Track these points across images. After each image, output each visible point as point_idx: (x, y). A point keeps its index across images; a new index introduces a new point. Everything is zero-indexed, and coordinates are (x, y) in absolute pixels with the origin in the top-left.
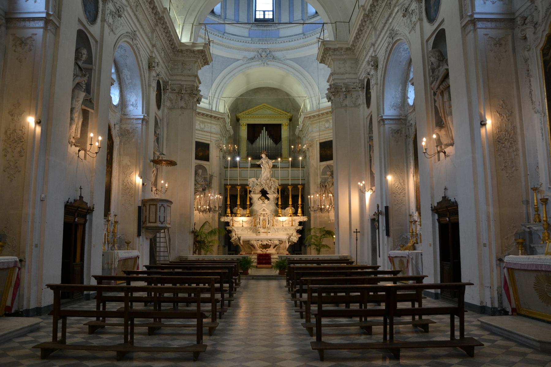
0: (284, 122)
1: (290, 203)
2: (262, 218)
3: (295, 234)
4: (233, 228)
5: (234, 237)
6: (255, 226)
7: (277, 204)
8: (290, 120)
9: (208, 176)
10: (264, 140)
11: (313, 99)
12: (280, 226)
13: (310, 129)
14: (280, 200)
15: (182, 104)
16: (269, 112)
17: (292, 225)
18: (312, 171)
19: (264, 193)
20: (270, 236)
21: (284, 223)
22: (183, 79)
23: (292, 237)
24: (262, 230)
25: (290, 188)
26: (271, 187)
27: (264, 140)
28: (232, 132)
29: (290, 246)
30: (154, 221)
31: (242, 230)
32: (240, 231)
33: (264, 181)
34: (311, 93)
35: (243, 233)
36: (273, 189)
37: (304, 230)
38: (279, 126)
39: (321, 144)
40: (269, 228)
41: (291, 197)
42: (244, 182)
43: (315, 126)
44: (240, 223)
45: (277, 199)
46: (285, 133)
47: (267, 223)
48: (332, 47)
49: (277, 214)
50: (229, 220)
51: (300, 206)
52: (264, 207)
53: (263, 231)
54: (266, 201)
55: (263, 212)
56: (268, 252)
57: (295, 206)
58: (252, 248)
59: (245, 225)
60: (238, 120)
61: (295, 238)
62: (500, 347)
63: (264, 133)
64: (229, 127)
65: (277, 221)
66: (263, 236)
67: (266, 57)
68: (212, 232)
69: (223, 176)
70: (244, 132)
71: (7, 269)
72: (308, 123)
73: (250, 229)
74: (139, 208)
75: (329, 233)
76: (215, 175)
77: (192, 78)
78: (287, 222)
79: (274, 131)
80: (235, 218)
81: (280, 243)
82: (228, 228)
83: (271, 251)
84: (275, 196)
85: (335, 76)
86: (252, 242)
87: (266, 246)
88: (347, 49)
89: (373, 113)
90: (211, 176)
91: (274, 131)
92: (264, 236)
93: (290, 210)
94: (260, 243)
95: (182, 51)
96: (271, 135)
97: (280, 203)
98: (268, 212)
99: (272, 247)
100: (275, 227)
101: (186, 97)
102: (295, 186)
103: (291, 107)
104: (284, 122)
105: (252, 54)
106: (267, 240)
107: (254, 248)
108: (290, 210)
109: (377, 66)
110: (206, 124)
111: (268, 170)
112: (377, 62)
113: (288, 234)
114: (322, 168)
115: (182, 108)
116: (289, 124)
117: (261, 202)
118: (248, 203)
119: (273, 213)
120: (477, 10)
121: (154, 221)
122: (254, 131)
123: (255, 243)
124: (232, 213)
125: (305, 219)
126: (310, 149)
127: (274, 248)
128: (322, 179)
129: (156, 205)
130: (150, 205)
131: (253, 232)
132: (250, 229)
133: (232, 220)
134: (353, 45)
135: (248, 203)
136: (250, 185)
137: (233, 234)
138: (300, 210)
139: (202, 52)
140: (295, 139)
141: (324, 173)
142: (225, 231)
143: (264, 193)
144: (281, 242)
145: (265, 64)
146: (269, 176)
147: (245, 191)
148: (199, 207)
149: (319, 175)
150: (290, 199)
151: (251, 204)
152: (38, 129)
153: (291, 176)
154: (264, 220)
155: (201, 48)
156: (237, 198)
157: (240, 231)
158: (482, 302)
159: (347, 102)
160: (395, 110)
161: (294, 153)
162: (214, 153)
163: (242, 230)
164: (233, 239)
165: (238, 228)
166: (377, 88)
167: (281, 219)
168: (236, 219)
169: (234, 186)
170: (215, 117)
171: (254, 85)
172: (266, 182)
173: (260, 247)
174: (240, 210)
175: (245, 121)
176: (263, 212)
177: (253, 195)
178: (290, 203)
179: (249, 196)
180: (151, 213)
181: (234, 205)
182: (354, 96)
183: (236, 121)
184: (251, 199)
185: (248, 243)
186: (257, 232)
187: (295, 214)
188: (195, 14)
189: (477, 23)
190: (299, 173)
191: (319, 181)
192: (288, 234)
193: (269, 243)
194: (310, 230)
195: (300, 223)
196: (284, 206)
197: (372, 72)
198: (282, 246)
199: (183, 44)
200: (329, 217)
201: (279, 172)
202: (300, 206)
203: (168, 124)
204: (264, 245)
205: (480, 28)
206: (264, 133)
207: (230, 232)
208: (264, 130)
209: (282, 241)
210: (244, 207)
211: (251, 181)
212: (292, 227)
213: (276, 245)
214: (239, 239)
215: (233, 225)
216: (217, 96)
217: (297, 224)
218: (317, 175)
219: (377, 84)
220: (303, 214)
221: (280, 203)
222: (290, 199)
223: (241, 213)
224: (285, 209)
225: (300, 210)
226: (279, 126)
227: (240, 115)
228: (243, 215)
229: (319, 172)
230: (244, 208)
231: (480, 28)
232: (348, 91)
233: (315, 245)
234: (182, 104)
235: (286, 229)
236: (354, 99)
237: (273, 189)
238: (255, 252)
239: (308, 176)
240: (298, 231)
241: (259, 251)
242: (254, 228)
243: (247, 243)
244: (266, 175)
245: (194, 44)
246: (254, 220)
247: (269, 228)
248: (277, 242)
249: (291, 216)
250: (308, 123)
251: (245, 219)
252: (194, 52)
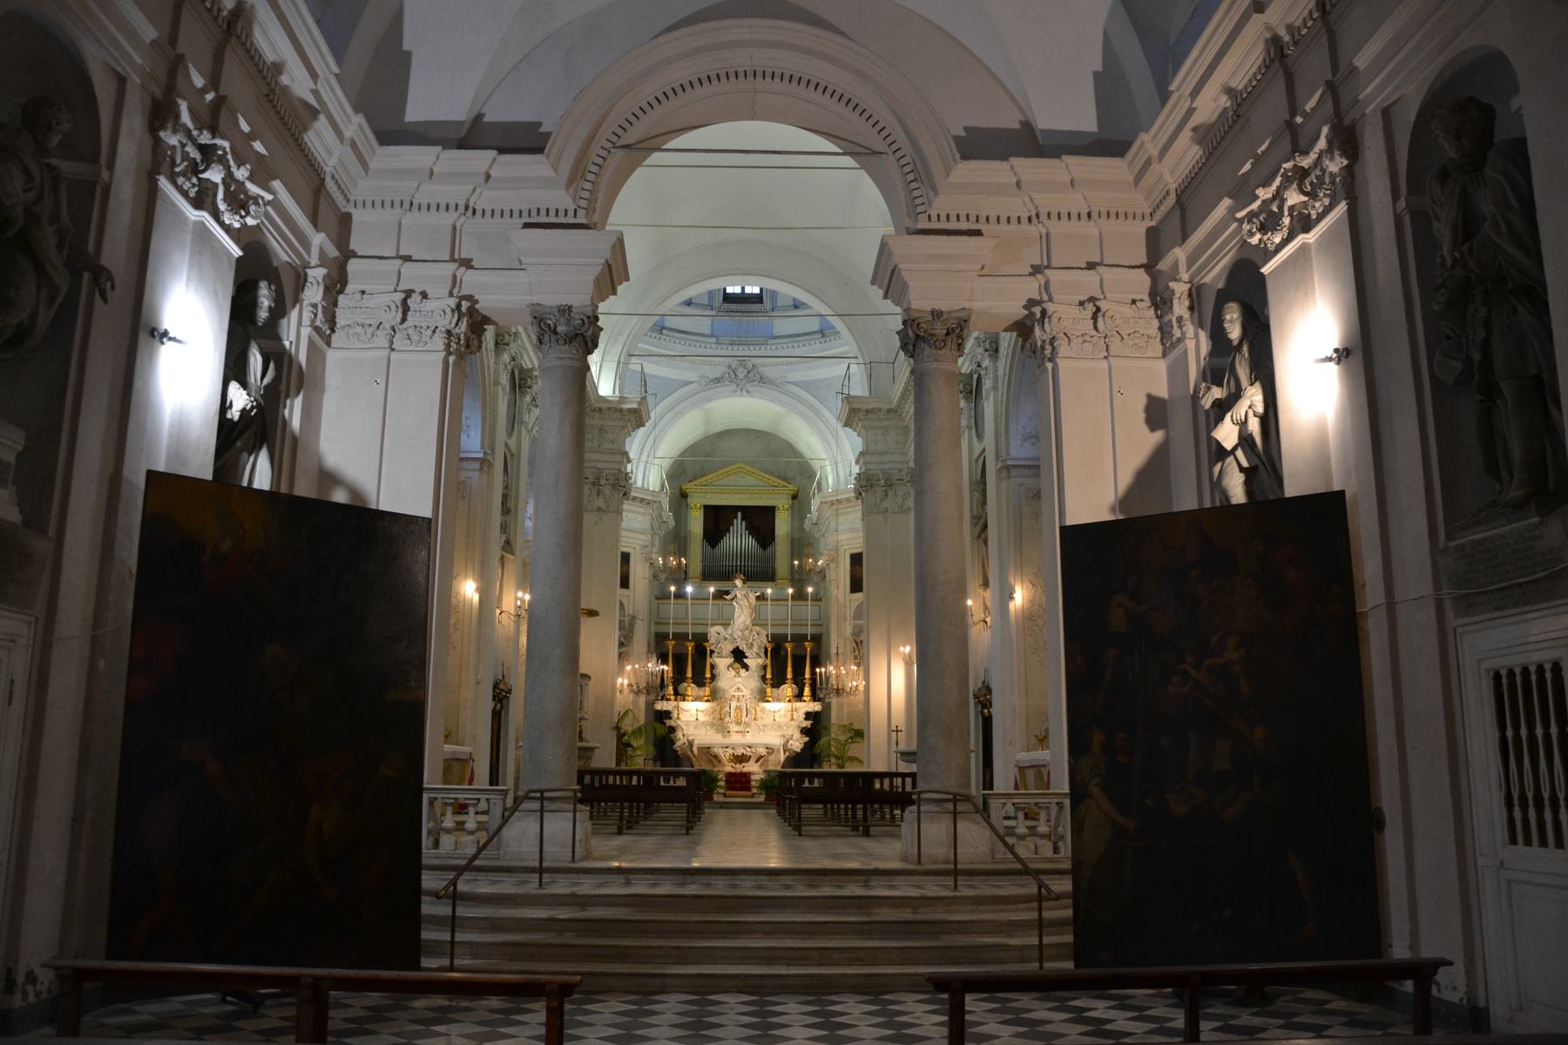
0: (781, 502)
1: (789, 676)
2: (734, 704)
3: (797, 735)
5: (681, 739)
7: (764, 678)
8: (794, 497)
10: (738, 539)
11: (840, 465)
12: (768, 720)
13: (832, 526)
14: (769, 670)
15: (600, 502)
16: (750, 480)
18: (834, 610)
19: (738, 655)
20: (749, 738)
22: (602, 458)
24: (734, 728)
25: (789, 646)
27: (738, 539)
28: (672, 523)
29: (787, 759)
34: (835, 458)
36: (755, 648)
37: (815, 727)
38: (770, 512)
40: (747, 725)
41: (793, 660)
42: (700, 630)
44: (692, 716)
45: (765, 667)
46: (782, 525)
48: (863, 407)
49: (763, 697)
51: (807, 682)
52: (738, 684)
54: (743, 671)
56: (745, 770)
57: (798, 681)
59: (702, 718)
60: (684, 496)
61: (797, 744)
63: (739, 525)
64: (668, 515)
65: (763, 710)
66: (735, 739)
67: (746, 377)
68: (638, 732)
69: (657, 618)
70: (696, 523)
71: (1532, 584)
72: (828, 512)
75: (859, 734)
77: (618, 458)
79: (760, 521)
82: (668, 722)
83: (752, 767)
84: (761, 661)
85: (868, 458)
87: (742, 759)
88: (889, 411)
89: (987, 453)
90: (633, 618)
91: (760, 521)
92: (739, 739)
93: (788, 689)
94: (730, 751)
95: (600, 410)
96: (753, 530)
97: (769, 676)
98: (746, 692)
99: (753, 760)
100: (760, 722)
101: (607, 491)
102: (799, 639)
103: (796, 474)
104: (781, 502)
105: (718, 372)
106: (744, 746)
108: (788, 689)
109: (997, 351)
111: (747, 611)
112: (997, 343)
114: (854, 606)
115: (599, 509)
116: (792, 507)
117: (733, 673)
118: (708, 675)
120: (1013, 453)
122: (718, 520)
123: (719, 751)
124: (676, 693)
125: (816, 707)
126: (832, 566)
128: (855, 626)
131: (718, 731)
132: (712, 725)
133: (677, 707)
134: (898, 406)
135: (708, 675)
136: (712, 640)
137: (680, 735)
138: (807, 690)
139: (635, 411)
140: (802, 544)
142: (661, 728)
143: (738, 655)
144: (770, 750)
146: (748, 622)
147: (702, 652)
148: (621, 677)
150: (789, 669)
151: (713, 677)
152: (476, 598)
153: (790, 616)
154: (738, 708)
155: (635, 406)
156: (688, 661)
159: (886, 504)
161: (798, 579)
162: (639, 572)
164: (678, 744)
165: (687, 723)
166: (995, 399)
167: (771, 706)
168: (684, 705)
169: (681, 637)
170: (642, 500)
171: (719, 427)
174: (691, 689)
175: (702, 497)
177: (717, 661)
178: (789, 676)
179: (709, 661)
181: (679, 677)
182: (900, 493)
183: (681, 499)
184: (713, 667)
186: (725, 731)
187: (799, 696)
188: (622, 339)
190: (808, 610)
191: (849, 631)
193: (748, 752)
194: (827, 729)
195: (808, 715)
196: (778, 681)
197: (986, 363)
198: (771, 758)
199: (603, 399)
201: (769, 609)
202: (807, 682)
206: (739, 525)
207: (672, 730)
208: (740, 529)
210: (699, 681)
211: (713, 631)
214: (691, 744)
216: (649, 462)
219: (995, 388)
220: (814, 698)
221: (769, 676)
222: (789, 669)
225: (807, 690)
226: (770, 512)
227: (688, 487)
228: (697, 699)
229: (850, 613)
232: (890, 485)
234: (600, 502)
235: (780, 726)
237: (755, 648)
239: (828, 619)
240: (804, 731)
241: (729, 769)
242: (720, 724)
244: (743, 617)
245: (622, 399)
247: (747, 725)
248: (763, 751)
250: (828, 512)
251: (703, 706)
252: (621, 411)
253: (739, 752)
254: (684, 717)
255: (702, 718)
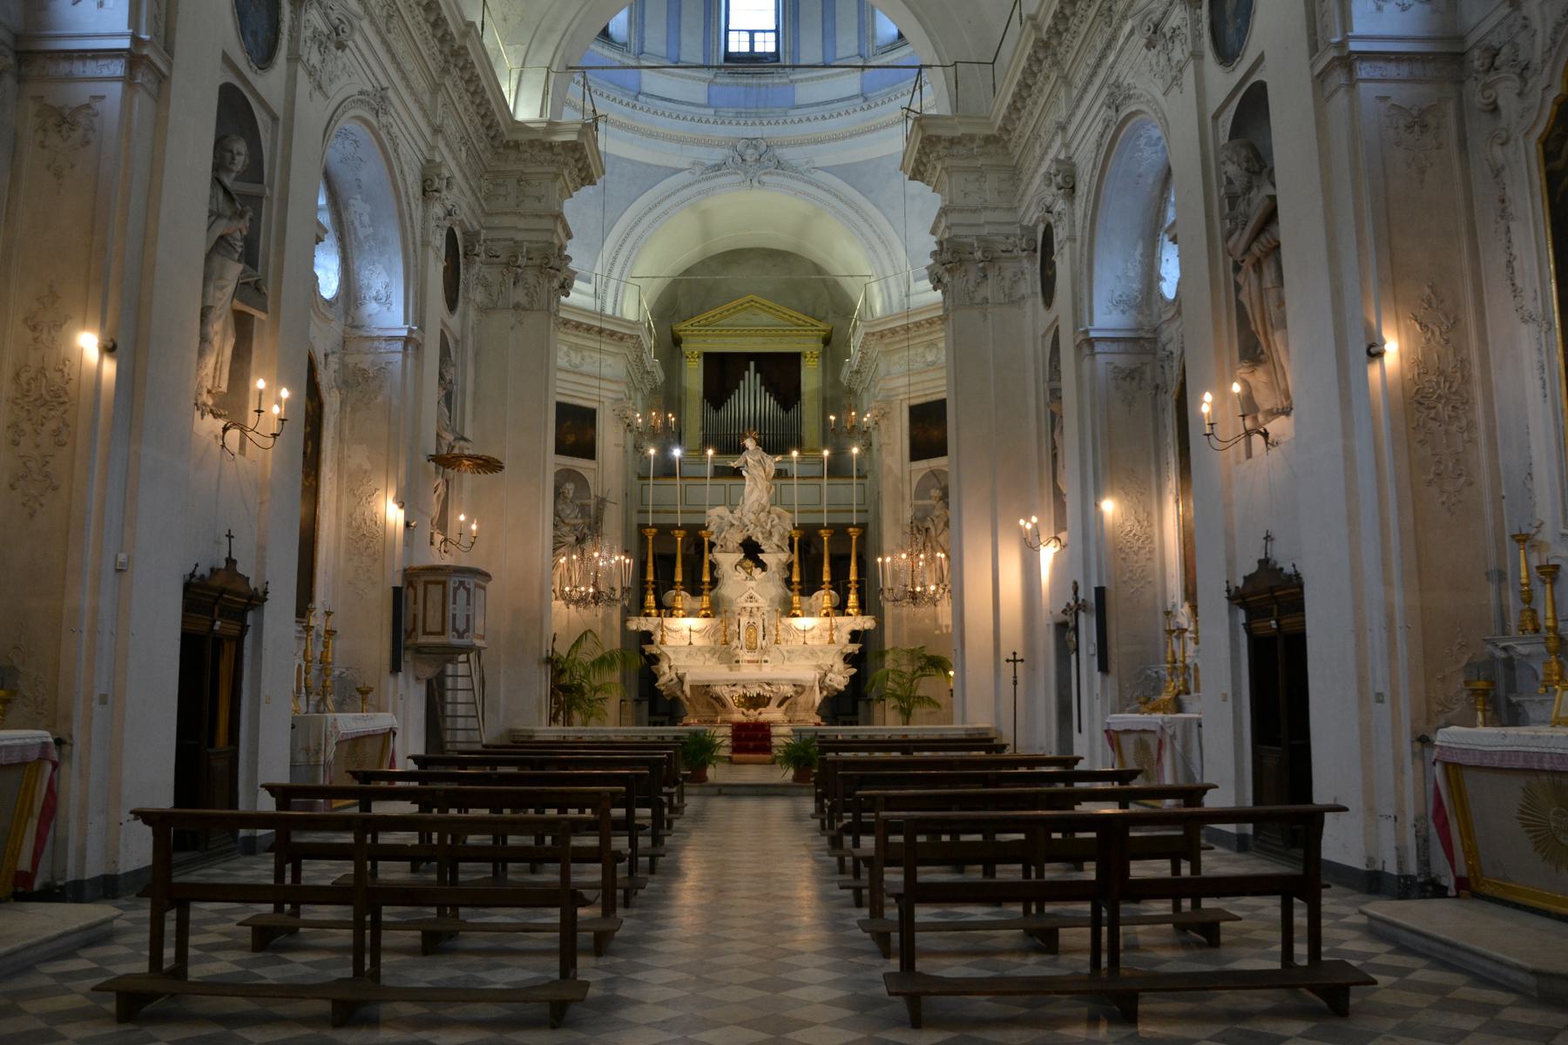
0: (809, 348)
1: (826, 578)
2: (744, 620)
3: (839, 665)
4: (664, 648)
5: (666, 674)
6: (726, 643)
7: (788, 582)
8: (827, 341)
9: (593, 502)
10: (751, 398)
11: (892, 281)
12: (797, 643)
13: (882, 368)
14: (796, 569)
15: (519, 296)
16: (765, 318)
17: (832, 642)
18: (887, 486)
19: (751, 550)
20: (767, 672)
21: (808, 635)
22: (522, 224)
23: (830, 675)
24: (745, 656)
25: (825, 535)
26: (770, 533)
27: (751, 398)
28: (660, 376)
29: (825, 700)
30: (439, 629)
31: (689, 655)
32: (682, 657)
33: (752, 517)
34: (885, 265)
35: (690, 662)
36: (776, 539)
37: (864, 654)
38: (794, 359)
39: (914, 410)
40: (764, 650)
41: (828, 560)
42: (694, 519)
43: (896, 358)
44: (683, 634)
45: (790, 566)
46: (811, 378)
47: (761, 634)
48: (945, 133)
49: (788, 610)
50: (650, 628)
51: (853, 587)
52: (750, 590)
53: (748, 657)
54: (757, 572)
55: (749, 605)
56: (762, 718)
57: (840, 585)
58: (718, 706)
59: (698, 641)
60: (677, 341)
61: (840, 678)
62: (1423, 987)
63: (752, 379)
64: (652, 362)
65: (788, 629)
66: (747, 672)
67: (756, 161)
68: (603, 662)
69: (634, 502)
70: (693, 377)
71: (20, 767)
72: (875, 349)
73: (713, 651)
74: (397, 592)
75: (937, 664)
76: (611, 498)
77: (547, 223)
78: (816, 632)
79: (780, 373)
80: (669, 622)
81: (796, 692)
82: (649, 649)
83: (772, 714)
84: (784, 557)
85: (954, 218)
86: (717, 689)
87: (758, 702)
88: (989, 140)
89: (1061, 323)
90: (602, 502)
91: (780, 373)
92: (751, 672)
93: (824, 598)
94: (741, 691)
95: (517, 145)
96: (770, 385)
97: (796, 578)
98: (763, 602)
99: (773, 704)
100: (783, 647)
101: (530, 277)
102: (839, 531)
103: (827, 304)
104: (809, 348)
105: (718, 155)
106: (760, 683)
107: (724, 705)
108: (824, 598)
109: (1073, 188)
110: (586, 353)
111: (762, 484)
112: (1073, 176)
113: (819, 667)
114: (916, 479)
115: (517, 306)
116: (823, 354)
117: (743, 574)
118: (706, 578)
119: (776, 606)
120: (1358, 28)
121: (439, 629)
122: (723, 372)
123: (724, 692)
124: (660, 605)
125: (867, 623)
126: (883, 424)
127: (779, 706)
128: (918, 509)
129: (444, 584)
130: (426, 583)
131: (721, 660)
132: (713, 651)
133: (661, 625)
134: (1004, 129)
135: (706, 578)
136: (712, 528)
137: (664, 666)
138: (853, 598)
139: (575, 147)
140: (839, 397)
141: (921, 491)
142: (642, 657)
143: (751, 550)
144: (800, 688)
145: (755, 183)
146: (765, 500)
147: (698, 544)
148: (566, 588)
149: (907, 497)
150: (826, 568)
151: (714, 582)
152: (109, 368)
153: (827, 501)
154: (751, 626)
155: (573, 137)
156: (675, 564)
157: (682, 657)
158: (1370, 860)
159: (987, 291)
160: (1124, 312)
161: (835, 437)
162: (609, 436)
163: (689, 655)
164: (662, 680)
165: (676, 649)
166: (1072, 251)
167: (801, 623)
168: (671, 623)
169: (665, 531)
170: (612, 334)
171: (723, 243)
172: (758, 519)
173: (741, 705)
174: (682, 599)
175: (697, 346)
176: (749, 605)
177: (719, 556)
178: (826, 578)
179: (707, 557)
180: (429, 605)
181: (665, 582)
182: (1008, 273)
183: (672, 346)
184: (713, 566)
185: (707, 693)
186: (731, 660)
187: (841, 608)
188: (554, 39)
189: (1358, 64)
190: (850, 491)
191: (908, 515)
192: (819, 667)
193: (766, 691)
194: (882, 654)
195: (855, 636)
196: (810, 586)
197: (1060, 206)
198: (801, 699)
199: (521, 127)
200: (936, 619)
201: (795, 490)
202: (853, 587)
203: (477, 354)
204: (751, 698)
205: (1365, 80)
206: (752, 379)
207: (654, 659)
208: (752, 370)
209: (803, 687)
210: (695, 589)
211: (715, 516)
212: (832, 647)
213: (786, 699)
214: (681, 680)
215: (662, 642)
216: (618, 273)
217: (846, 637)
218: (903, 499)
219: (1072, 239)
220: (863, 609)
221: (796, 578)
222: (826, 568)
223: (687, 606)
224: (810, 595)
225: (853, 598)
226: (794, 359)
227: (682, 327)
228: (690, 613)
229: (908, 490)
230: (696, 592)
231: (1365, 80)
232: (991, 259)
233: (897, 697)
234: (519, 296)
235: (813, 653)
236: (1007, 283)
237: (776, 539)
238: (727, 717)
239: (878, 502)
240: (849, 659)
241: (738, 716)
242: (724, 649)
243: (704, 691)
244: (757, 498)
245: (552, 126)
246: (722, 627)
247: (764, 650)
248: (788, 690)
249: (827, 615)
250: (875, 349)
251: (697, 623)
252: (551, 147)
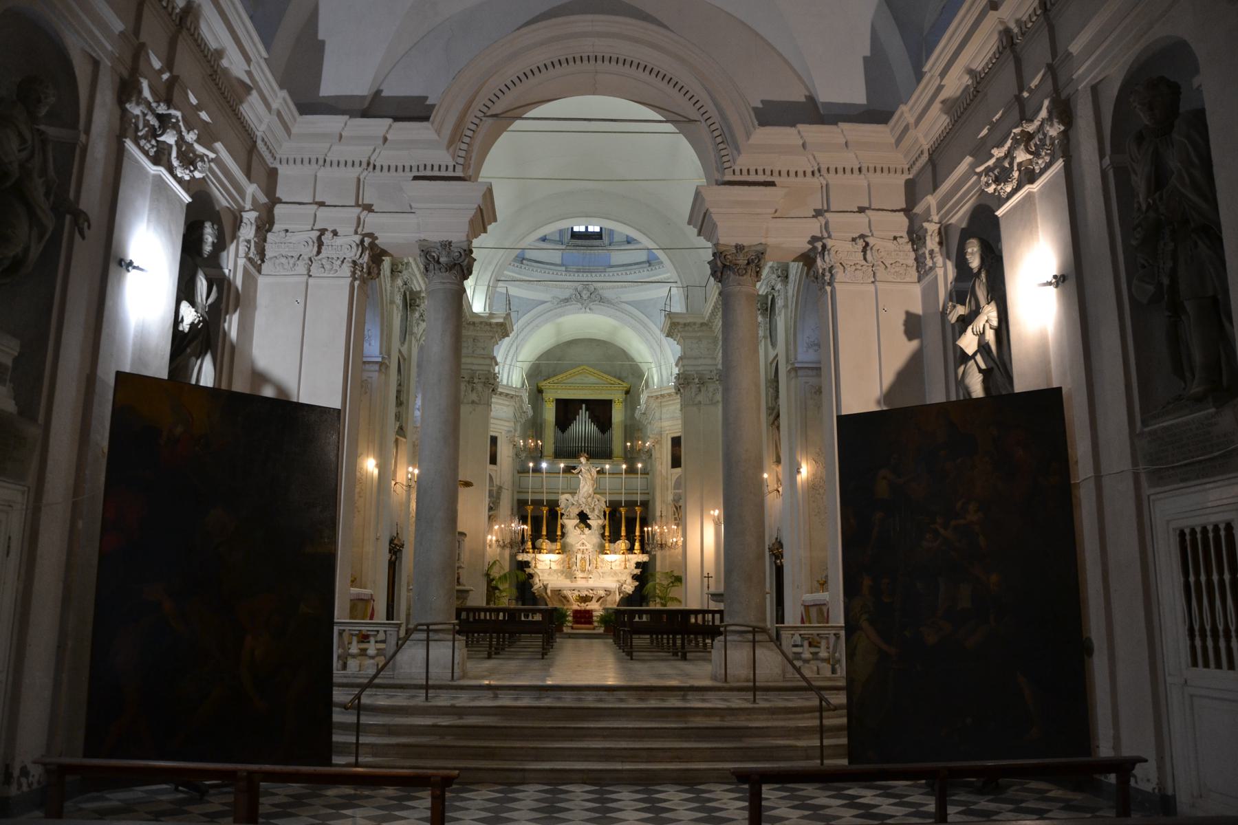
0: (617, 396)
1: (623, 533)
2: (579, 556)
3: (629, 580)
5: (537, 584)
7: (603, 535)
8: (627, 392)
10: (583, 426)
11: (663, 367)
12: (607, 568)
13: (657, 415)
14: (607, 529)
15: (474, 397)
16: (592, 379)
18: (658, 481)
19: (583, 517)
20: (591, 583)
22: (475, 361)
24: (579, 574)
25: (623, 510)
27: (583, 426)
28: (530, 413)
29: (622, 599)
34: (659, 361)
36: (596, 512)
37: (644, 574)
38: (608, 404)
40: (590, 572)
41: (626, 521)
42: (552, 497)
44: (547, 565)
45: (604, 527)
46: (618, 415)
48: (682, 321)
49: (602, 550)
51: (638, 538)
52: (582, 540)
54: (586, 530)
56: (588, 608)
57: (630, 538)
59: (554, 567)
60: (540, 391)
61: (630, 587)
63: (583, 414)
64: (528, 407)
65: (602, 561)
66: (580, 583)
67: (589, 298)
68: (504, 578)
69: (519, 488)
70: (550, 413)
71: (1210, 461)
72: (654, 404)
75: (678, 580)
77: (488, 361)
79: (600, 411)
82: (528, 570)
83: (593, 606)
84: (601, 522)
85: (686, 362)
87: (586, 599)
88: (702, 324)
89: (779, 358)
90: (500, 488)
91: (600, 411)
92: (584, 583)
93: (622, 544)
94: (577, 593)
95: (474, 323)
96: (595, 418)
97: (607, 534)
98: (589, 546)
99: (594, 600)
100: (600, 570)
101: (479, 387)
102: (631, 504)
103: (629, 374)
104: (617, 396)
105: (567, 293)
106: (587, 589)
108: (622, 544)
109: (787, 277)
111: (590, 483)
112: (787, 271)
114: (674, 478)
115: (473, 402)
116: (625, 400)
117: (579, 531)
118: (559, 533)
120: (800, 358)
122: (567, 410)
123: (568, 593)
124: (534, 547)
125: (644, 558)
126: (657, 447)
128: (675, 495)
131: (567, 577)
132: (562, 572)
133: (535, 558)
134: (709, 321)
135: (559, 533)
136: (562, 505)
137: (537, 580)
138: (637, 545)
139: (501, 325)
140: (633, 430)
142: (522, 575)
143: (583, 517)
144: (608, 592)
146: (591, 491)
147: (554, 515)
150: (623, 528)
151: (563, 535)
152: (376, 472)
153: (624, 487)
154: (583, 559)
155: (501, 320)
156: (544, 522)
159: (700, 398)
161: (630, 457)
162: (504, 452)
164: (536, 587)
165: (543, 571)
166: (786, 315)
167: (609, 558)
168: (540, 557)
169: (537, 503)
170: (507, 395)
171: (567, 337)
174: (545, 544)
175: (554, 393)
177: (566, 522)
178: (623, 533)
179: (560, 522)
181: (536, 534)
182: (711, 389)
183: (537, 394)
184: (563, 526)
186: (572, 577)
187: (631, 550)
188: (491, 268)
190: (638, 482)
191: (670, 498)
193: (590, 594)
194: (653, 575)
195: (638, 565)
196: (615, 537)
197: (779, 286)
198: (609, 598)
199: (476, 315)
201: (607, 481)
202: (638, 538)
206: (583, 414)
207: (531, 576)
208: (584, 418)
210: (552, 538)
211: (563, 499)
214: (545, 587)
216: (512, 365)
219: (786, 306)
220: (643, 551)
221: (607, 534)
222: (623, 528)
225: (637, 545)
226: (608, 404)
227: (543, 384)
228: (550, 552)
229: (671, 484)
232: (702, 383)
234: (474, 397)
235: (616, 574)
237: (596, 512)
239: (654, 489)
240: (635, 577)
241: (575, 607)
242: (568, 572)
244: (587, 487)
245: (491, 315)
247: (590, 572)
248: (602, 593)
250: (654, 404)
251: (555, 557)
252: (491, 324)
253: (584, 593)
254: (540, 566)
255: (554, 567)
